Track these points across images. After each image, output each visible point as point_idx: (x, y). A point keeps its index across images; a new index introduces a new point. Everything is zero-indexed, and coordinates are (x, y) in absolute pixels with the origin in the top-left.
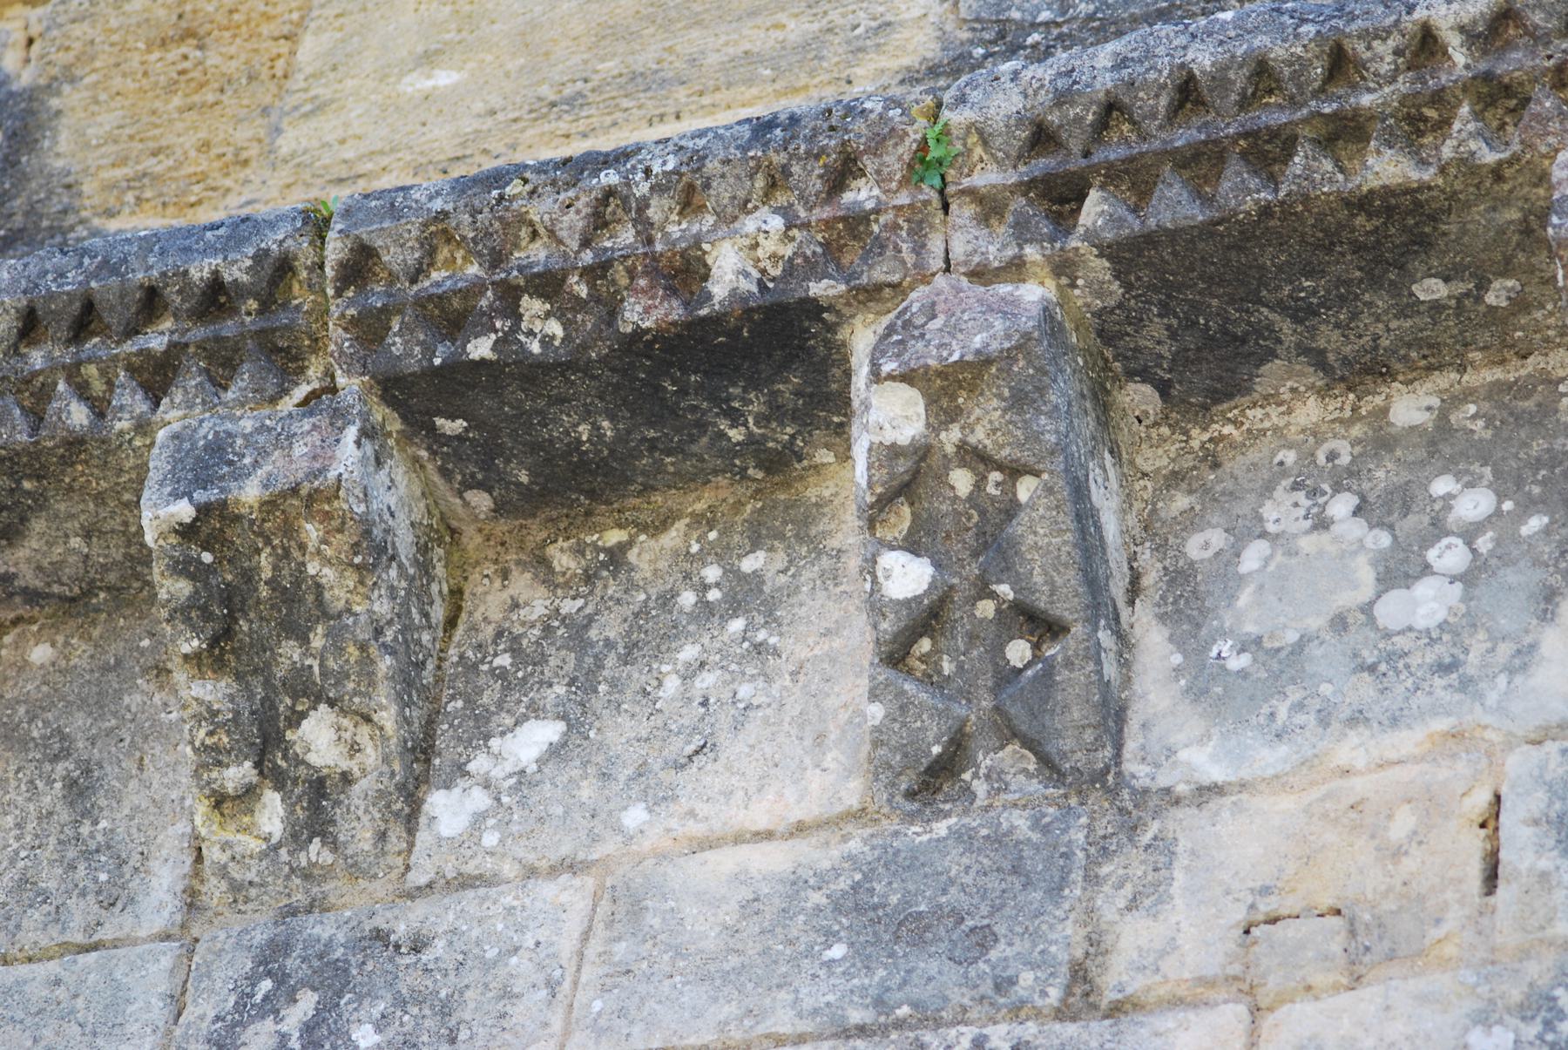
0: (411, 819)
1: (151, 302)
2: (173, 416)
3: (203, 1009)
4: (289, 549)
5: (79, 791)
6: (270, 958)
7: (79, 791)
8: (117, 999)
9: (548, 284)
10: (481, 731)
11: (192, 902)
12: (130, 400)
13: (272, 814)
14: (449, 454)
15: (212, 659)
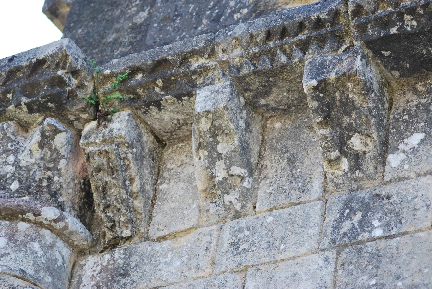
0: (383, 161)
1: (301, 26)
2: (309, 57)
3: (331, 218)
4: (344, 91)
5: (291, 161)
6: (348, 203)
7: (291, 161)
8: (307, 217)
9: (412, 11)
10: (401, 137)
11: (325, 190)
12: (297, 54)
13: (345, 164)
14: (386, 61)
15: (325, 123)
